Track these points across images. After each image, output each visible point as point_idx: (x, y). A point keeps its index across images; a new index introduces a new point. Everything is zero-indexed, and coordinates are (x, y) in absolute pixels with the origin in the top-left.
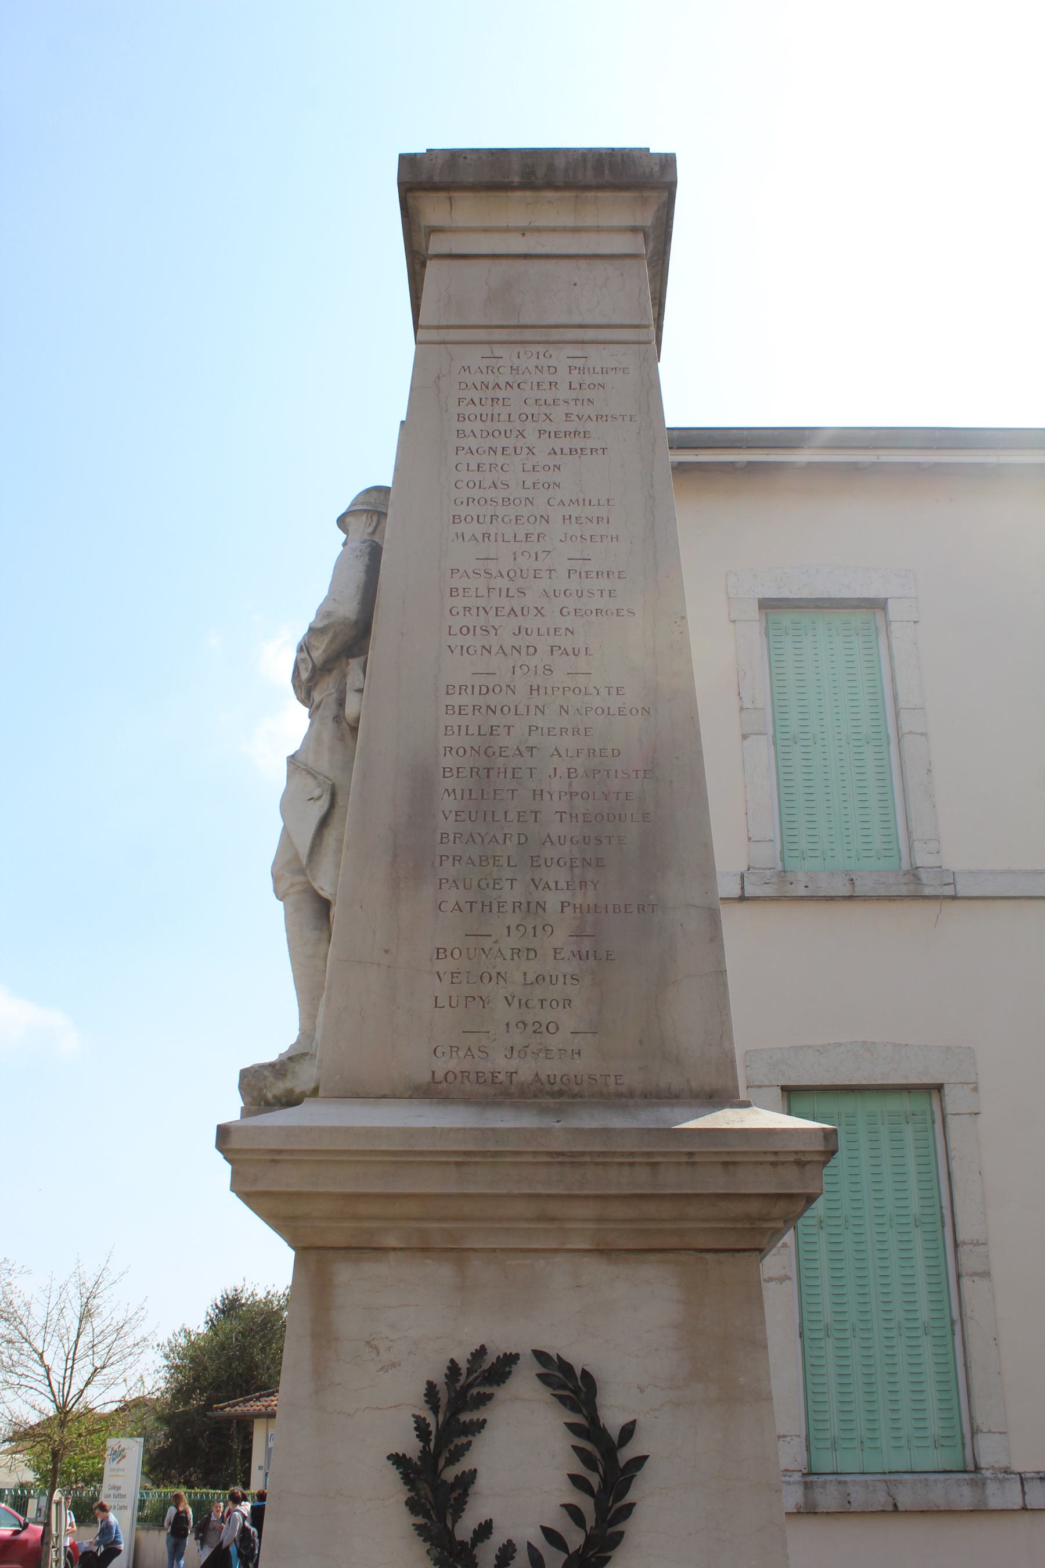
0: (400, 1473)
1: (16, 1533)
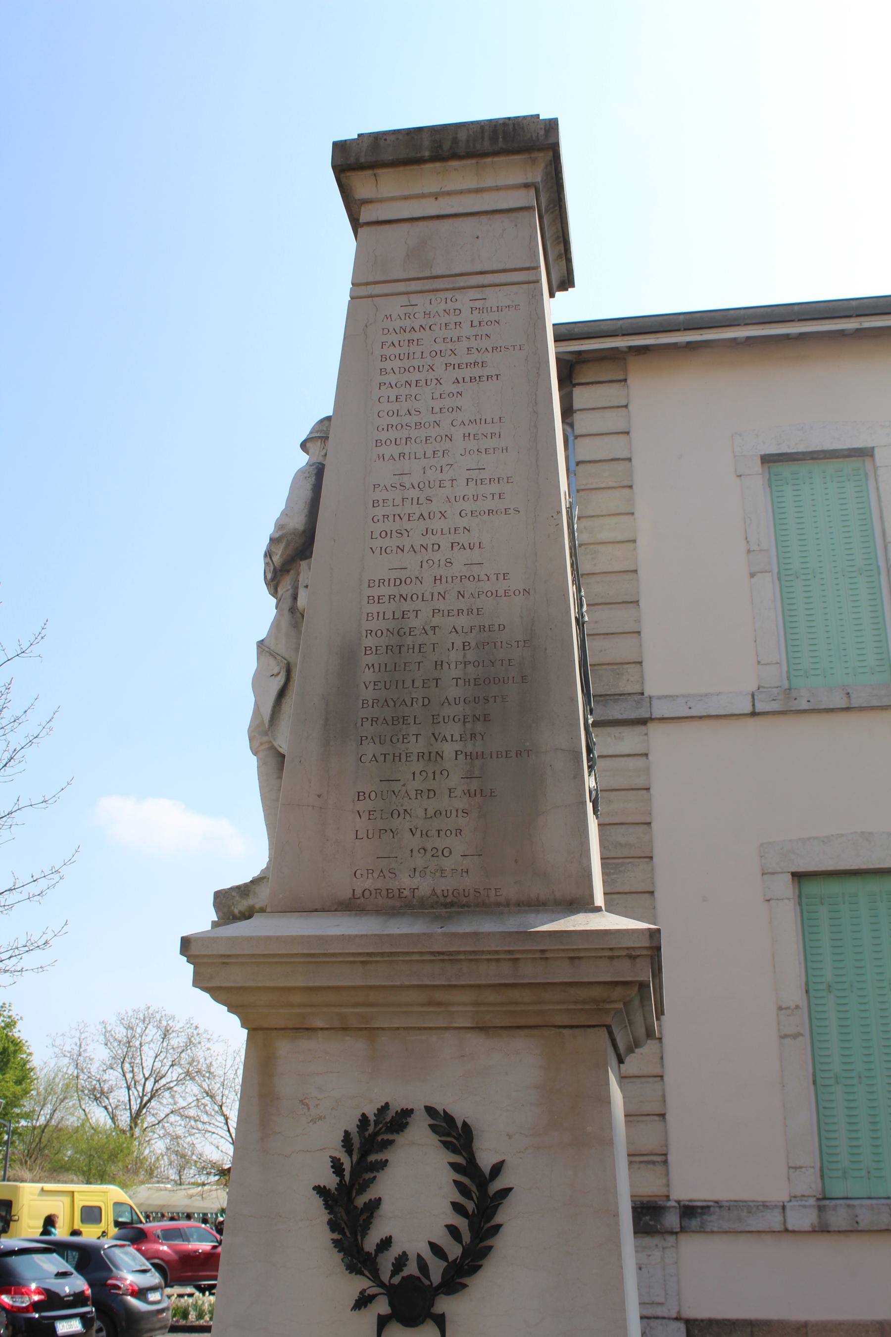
1: (214, 1247)
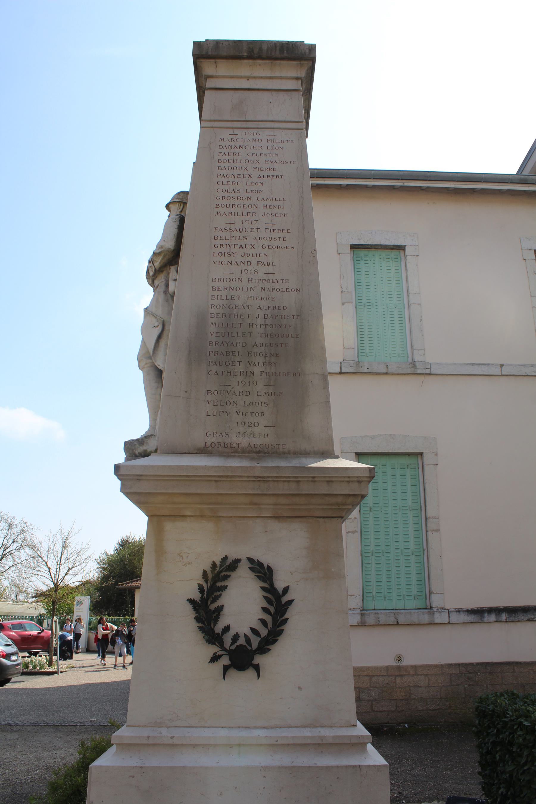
0: (192, 606)
1: (39, 633)
